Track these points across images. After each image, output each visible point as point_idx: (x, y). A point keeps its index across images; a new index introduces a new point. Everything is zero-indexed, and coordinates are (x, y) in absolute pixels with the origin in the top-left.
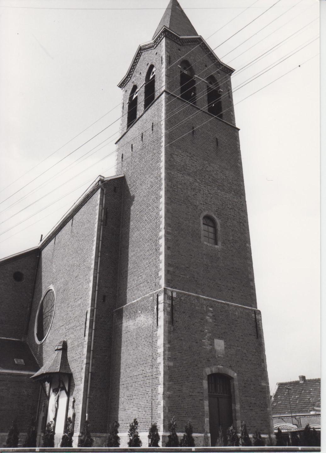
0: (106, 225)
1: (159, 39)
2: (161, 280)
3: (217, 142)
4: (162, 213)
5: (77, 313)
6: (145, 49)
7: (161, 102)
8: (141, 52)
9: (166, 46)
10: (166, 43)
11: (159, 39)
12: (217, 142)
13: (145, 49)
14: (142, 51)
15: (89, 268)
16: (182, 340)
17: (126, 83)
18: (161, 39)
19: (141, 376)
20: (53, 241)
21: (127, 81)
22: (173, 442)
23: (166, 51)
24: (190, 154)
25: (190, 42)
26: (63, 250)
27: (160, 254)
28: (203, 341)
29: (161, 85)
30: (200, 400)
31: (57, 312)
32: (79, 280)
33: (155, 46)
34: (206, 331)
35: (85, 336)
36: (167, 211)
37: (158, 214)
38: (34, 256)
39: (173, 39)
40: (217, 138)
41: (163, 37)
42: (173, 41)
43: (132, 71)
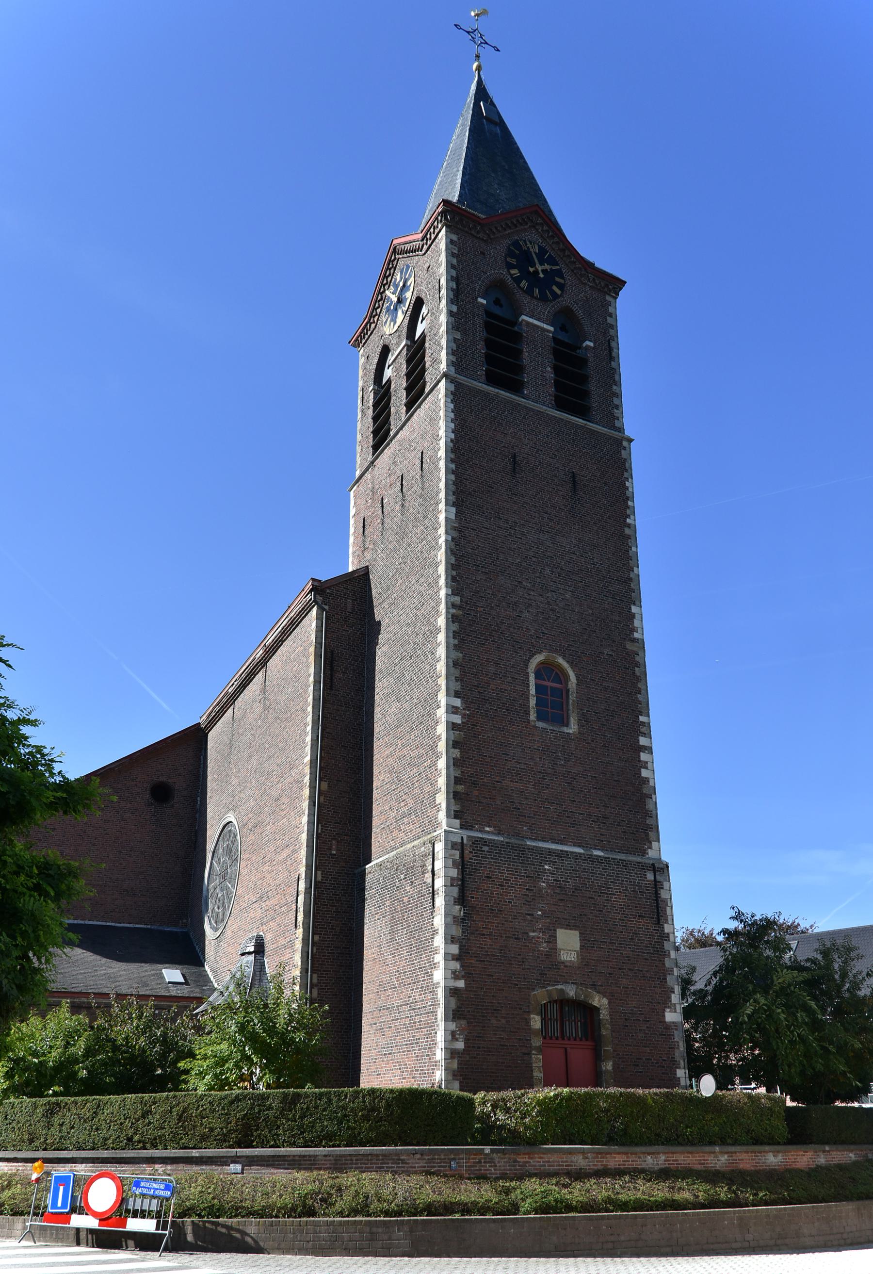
0: (331, 689)
1: (432, 230)
2: (440, 812)
3: (574, 482)
4: (441, 667)
5: (281, 877)
6: (402, 252)
7: (438, 398)
8: (395, 258)
9: (450, 254)
10: (450, 243)
11: (432, 230)
12: (574, 482)
13: (402, 252)
14: (397, 256)
15: (300, 782)
16: (484, 935)
17: (367, 337)
18: (437, 231)
19: (406, 1008)
20: (230, 711)
21: (369, 333)
22: (715, 1061)
23: (450, 266)
24: (507, 521)
25: (510, 228)
26: (249, 736)
27: (438, 757)
28: (532, 934)
29: (439, 359)
30: (524, 1054)
31: (244, 872)
32: (283, 807)
33: (425, 247)
34: (540, 913)
35: (296, 927)
36: (453, 664)
37: (433, 667)
38: (194, 740)
39: (466, 229)
40: (573, 472)
41: (440, 226)
42: (467, 232)
43: (379, 307)
